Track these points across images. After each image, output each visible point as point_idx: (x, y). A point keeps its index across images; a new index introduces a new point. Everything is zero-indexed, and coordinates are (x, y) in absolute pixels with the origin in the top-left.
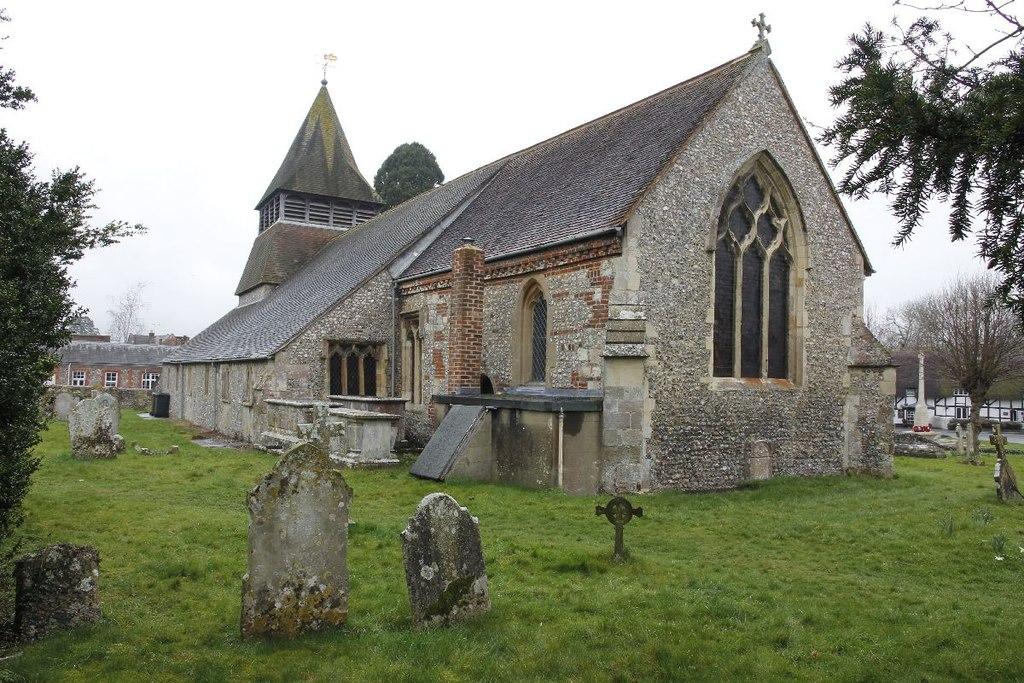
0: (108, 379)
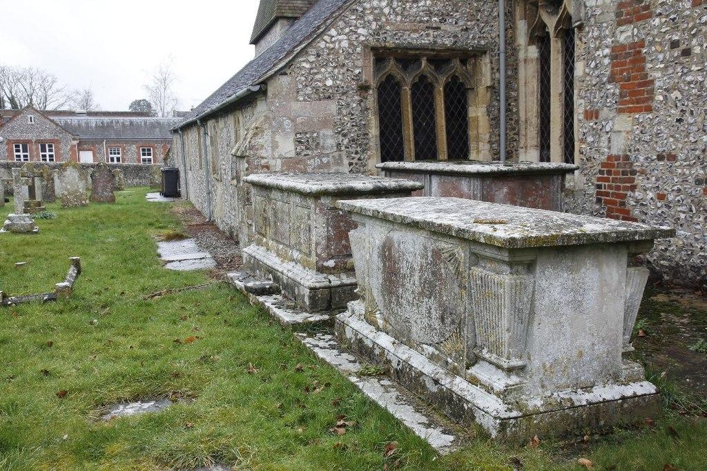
0: (144, 154)
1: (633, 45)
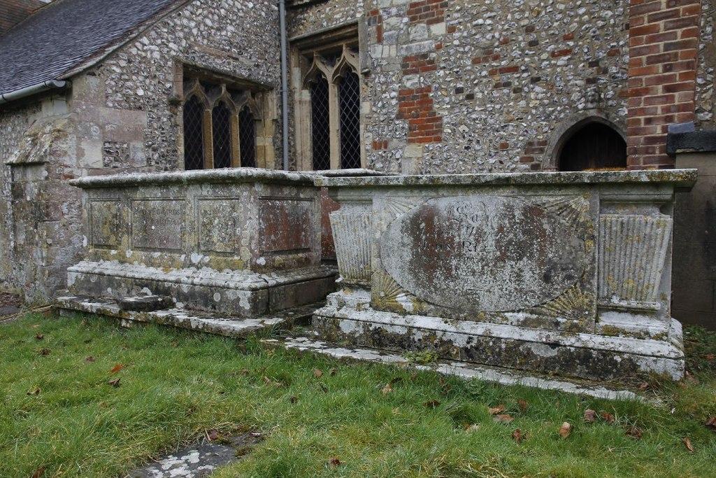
1: (421, 90)
